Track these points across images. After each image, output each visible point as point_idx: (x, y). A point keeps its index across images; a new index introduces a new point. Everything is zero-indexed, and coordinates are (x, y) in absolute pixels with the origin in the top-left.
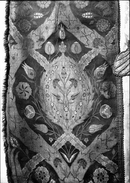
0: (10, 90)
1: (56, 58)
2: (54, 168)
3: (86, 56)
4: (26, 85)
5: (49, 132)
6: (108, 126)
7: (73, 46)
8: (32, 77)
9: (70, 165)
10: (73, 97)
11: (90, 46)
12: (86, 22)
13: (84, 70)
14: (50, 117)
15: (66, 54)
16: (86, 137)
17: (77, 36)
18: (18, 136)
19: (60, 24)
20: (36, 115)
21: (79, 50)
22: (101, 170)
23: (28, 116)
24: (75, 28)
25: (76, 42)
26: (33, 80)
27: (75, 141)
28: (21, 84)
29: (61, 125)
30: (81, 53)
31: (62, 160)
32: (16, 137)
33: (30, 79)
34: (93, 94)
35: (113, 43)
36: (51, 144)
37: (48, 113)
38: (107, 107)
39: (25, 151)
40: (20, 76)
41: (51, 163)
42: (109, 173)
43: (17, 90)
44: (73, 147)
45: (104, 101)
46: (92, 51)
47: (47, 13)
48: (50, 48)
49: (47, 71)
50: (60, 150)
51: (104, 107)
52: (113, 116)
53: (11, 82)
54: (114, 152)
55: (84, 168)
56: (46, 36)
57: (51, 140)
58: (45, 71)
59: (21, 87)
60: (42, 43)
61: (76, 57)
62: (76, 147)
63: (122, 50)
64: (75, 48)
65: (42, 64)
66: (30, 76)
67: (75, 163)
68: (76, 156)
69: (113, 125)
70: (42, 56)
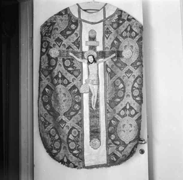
0: (40, 98)
3: (69, 85)
6: (78, 113)
10: (64, 101)
12: (69, 71)
13: (68, 91)
14: (121, 138)
16: (69, 117)
17: (66, 77)
19: (59, 72)
21: (67, 83)
23: (48, 109)
24: (65, 74)
25: (65, 79)
26: (115, 125)
30: (134, 114)
34: (72, 100)
38: (77, 105)
39: (46, 122)
47: (121, 99)
48: (123, 113)
51: (76, 106)
52: (80, 109)
53: (41, 95)
54: (80, 123)
55: (68, 129)
59: (47, 100)
61: (65, 85)
62: (65, 121)
63: (83, 83)
64: (65, 82)
66: (114, 124)
67: (65, 127)
68: (65, 125)
69: (80, 112)
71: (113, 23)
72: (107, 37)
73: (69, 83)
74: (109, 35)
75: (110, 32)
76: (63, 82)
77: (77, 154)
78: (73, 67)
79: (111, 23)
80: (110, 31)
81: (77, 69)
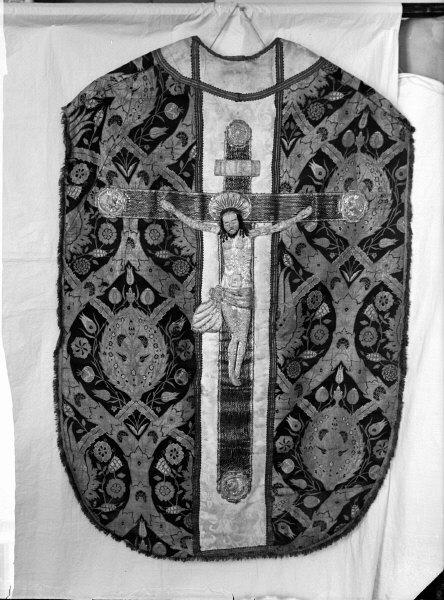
1: (122, 308)
2: (119, 443)
4: (85, 341)
5: (330, 246)
7: (144, 293)
8: (320, 177)
9: (138, 438)
11: (166, 295)
15: (135, 305)
16: (158, 405)
18: (73, 403)
19: (126, 266)
20: (96, 379)
22: (176, 446)
27: (146, 411)
28: (77, 339)
29: (126, 391)
31: (129, 433)
32: (290, 254)
33: (317, 180)
35: (193, 291)
36: (113, 414)
37: (110, 377)
40: (77, 329)
41: (114, 437)
42: (184, 449)
43: (73, 347)
44: (143, 416)
45: (181, 364)
46: (397, 144)
49: (340, 169)
50: (126, 421)
51: (180, 372)
56: (111, 280)
57: (114, 409)
58: (108, 324)
60: (106, 288)
65: (104, 315)
68: (360, 273)
69: (190, 393)
70: (104, 305)
71: (310, 102)
72: (288, 148)
73: (159, 300)
74: (294, 143)
75: (298, 134)
76: (139, 300)
77: (179, 514)
78: (171, 249)
79: (303, 102)
80: (298, 130)
81: (183, 252)
